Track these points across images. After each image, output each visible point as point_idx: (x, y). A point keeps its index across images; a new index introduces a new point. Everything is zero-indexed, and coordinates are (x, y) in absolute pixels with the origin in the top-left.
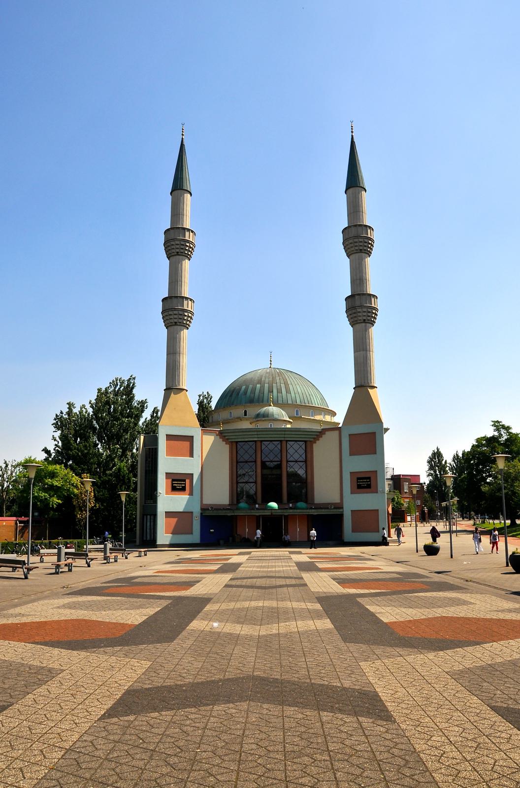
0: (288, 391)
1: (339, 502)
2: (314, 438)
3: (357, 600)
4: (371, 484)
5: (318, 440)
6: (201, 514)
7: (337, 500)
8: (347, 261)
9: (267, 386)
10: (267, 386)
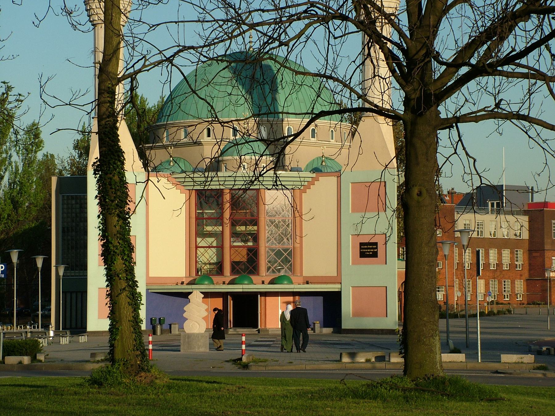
1: (343, 327)
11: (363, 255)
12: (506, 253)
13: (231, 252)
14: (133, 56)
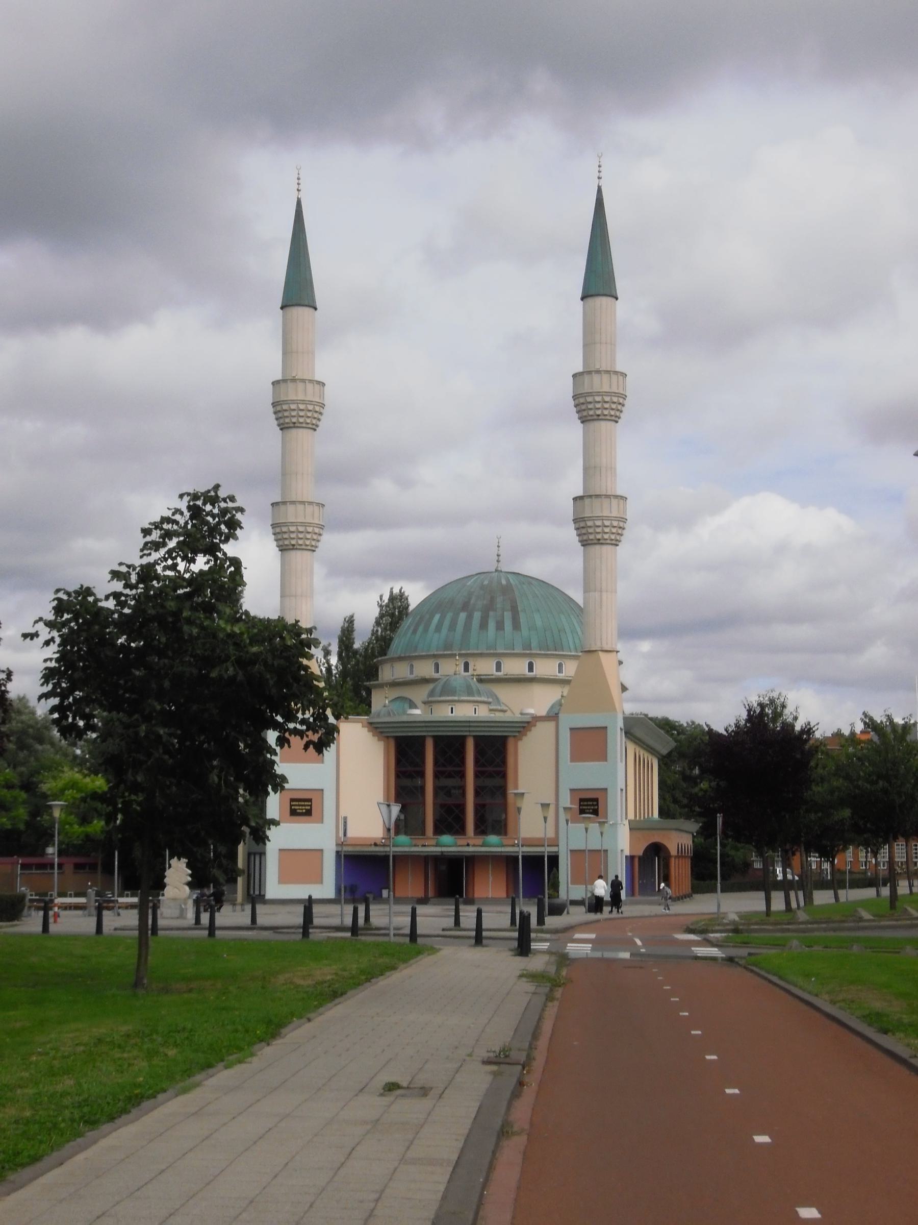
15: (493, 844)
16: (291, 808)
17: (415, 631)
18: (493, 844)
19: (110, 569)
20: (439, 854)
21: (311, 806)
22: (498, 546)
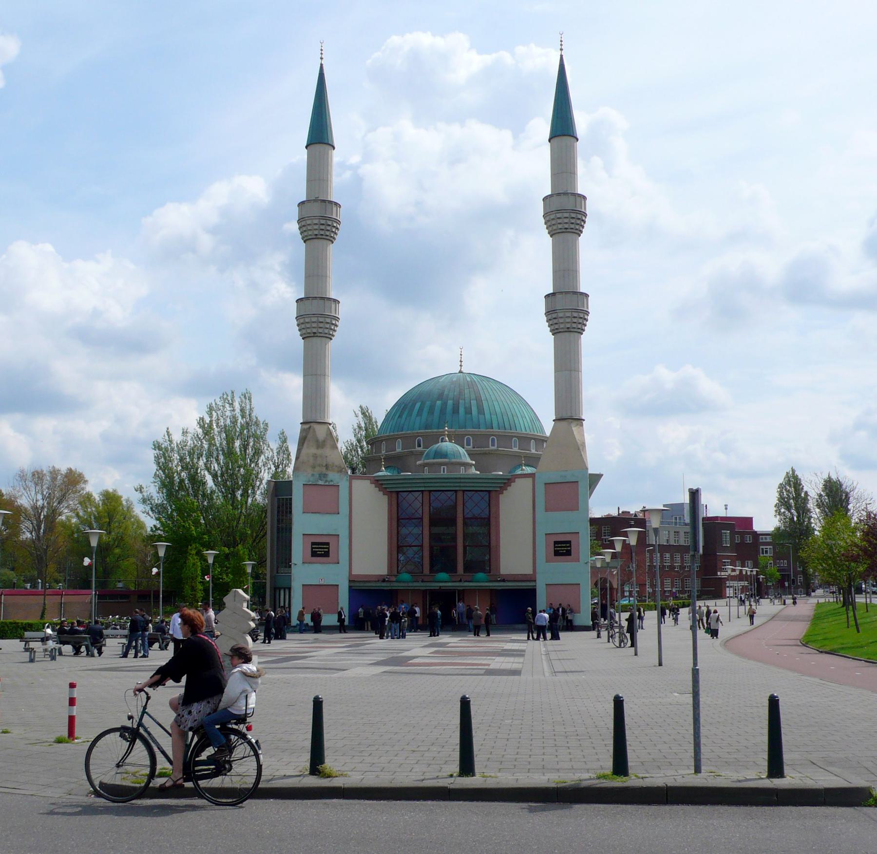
0: (481, 411)
1: (532, 573)
2: (505, 483)
3: (229, 711)
4: (572, 550)
5: (506, 490)
6: (350, 587)
7: (529, 571)
8: (548, 240)
9: (450, 402)
10: (450, 402)
11: (314, 554)
12: (678, 557)
13: (421, 512)
14: (44, 595)
15: (481, 580)
16: (312, 550)
17: (400, 416)
18: (481, 580)
19: (77, 686)
20: (438, 588)
21: (328, 548)
22: (461, 355)
